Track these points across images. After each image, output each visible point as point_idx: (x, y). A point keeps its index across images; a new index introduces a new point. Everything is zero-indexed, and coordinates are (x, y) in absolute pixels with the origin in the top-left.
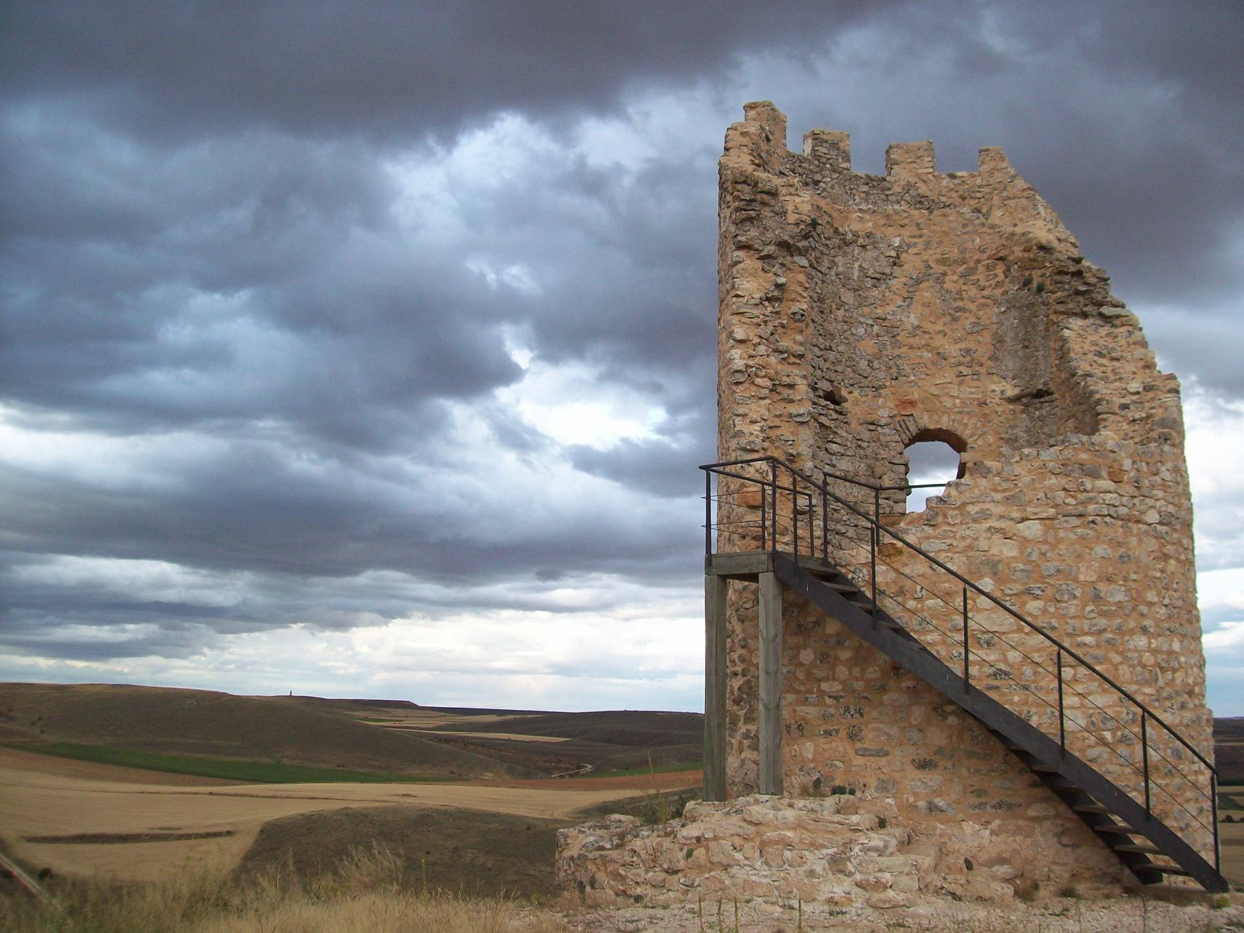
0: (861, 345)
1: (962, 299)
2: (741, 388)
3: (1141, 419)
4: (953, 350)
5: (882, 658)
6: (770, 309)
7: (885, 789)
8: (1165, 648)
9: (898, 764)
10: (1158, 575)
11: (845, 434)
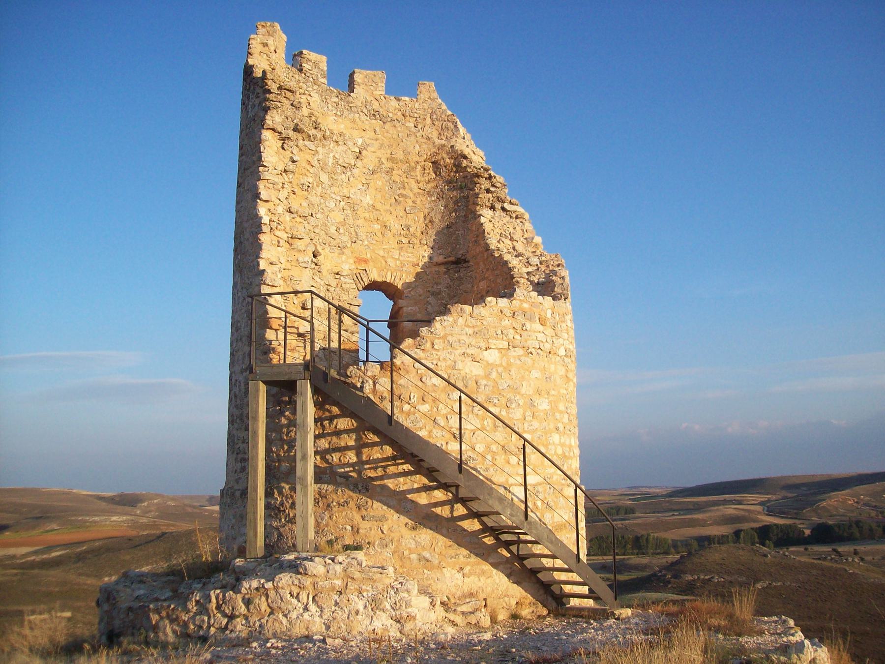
0: (332, 215)
1: (404, 188)
4: (395, 226)
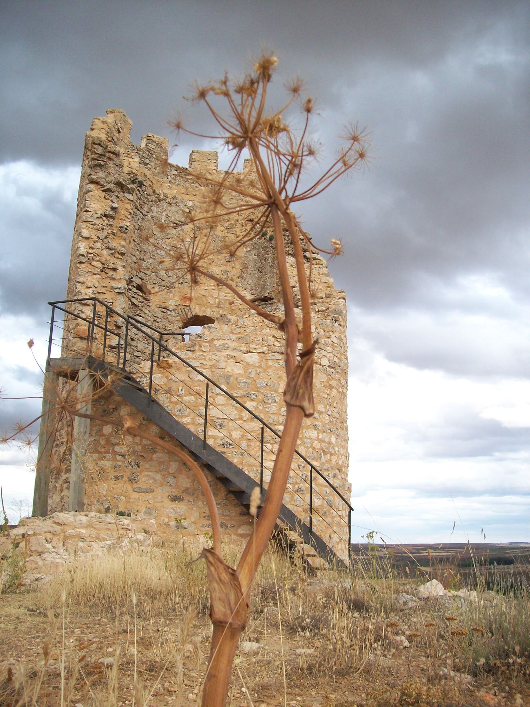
2: (83, 266)
3: (323, 311)
5: (154, 429)
6: (106, 222)
7: (150, 513)
8: (327, 440)
9: (159, 498)
10: (326, 396)
11: (147, 312)
